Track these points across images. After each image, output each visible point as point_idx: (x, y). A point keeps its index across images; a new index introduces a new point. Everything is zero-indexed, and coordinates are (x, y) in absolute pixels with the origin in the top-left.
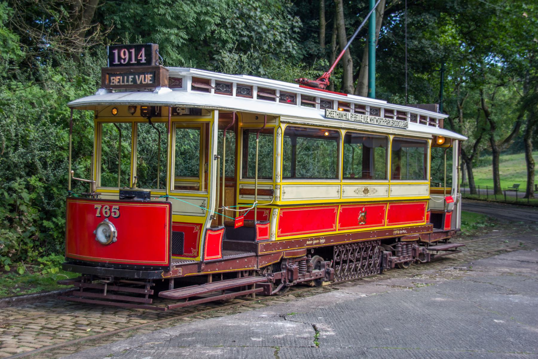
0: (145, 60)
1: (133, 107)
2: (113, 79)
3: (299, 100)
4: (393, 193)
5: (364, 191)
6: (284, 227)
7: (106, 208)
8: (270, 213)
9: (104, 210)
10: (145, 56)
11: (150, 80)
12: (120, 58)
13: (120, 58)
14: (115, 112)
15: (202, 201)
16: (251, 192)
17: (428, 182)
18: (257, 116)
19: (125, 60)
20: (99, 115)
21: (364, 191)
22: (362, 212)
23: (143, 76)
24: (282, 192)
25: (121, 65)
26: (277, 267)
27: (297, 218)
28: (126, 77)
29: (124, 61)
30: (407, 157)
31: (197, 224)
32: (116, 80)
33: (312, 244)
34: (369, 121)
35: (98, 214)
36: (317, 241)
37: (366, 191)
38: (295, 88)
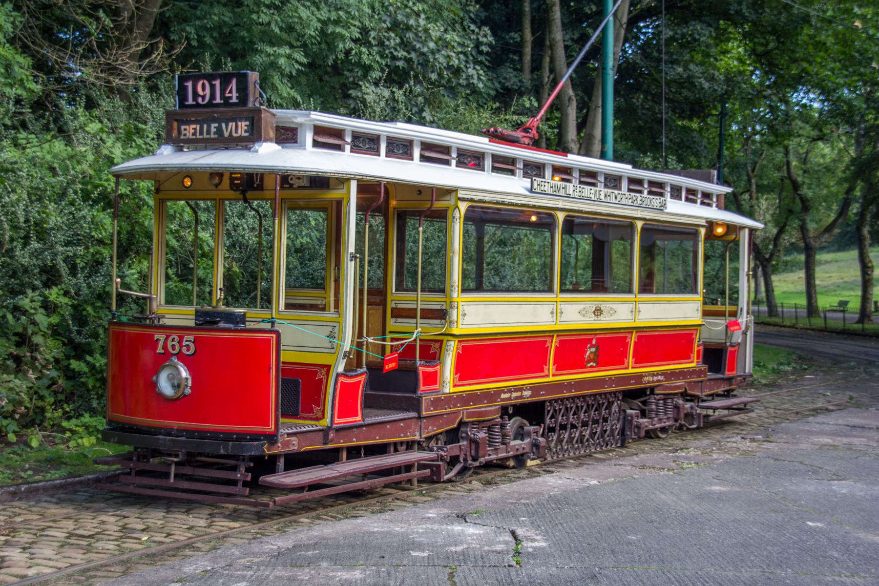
0: (237, 98)
1: (216, 174)
2: (185, 130)
3: (488, 163)
4: (642, 316)
5: (594, 312)
6: (464, 371)
7: (173, 340)
8: (441, 347)
9: (170, 343)
10: (237, 92)
11: (246, 131)
12: (196, 95)
13: (196, 95)
14: (188, 182)
15: (330, 329)
16: (410, 314)
17: (699, 297)
18: (420, 190)
19: (203, 97)
20: (162, 188)
21: (594, 312)
22: (592, 346)
23: (234, 124)
24: (460, 313)
25: (198, 105)
26: (453, 436)
27: (486, 356)
28: (205, 126)
29: (203, 100)
30: (664, 256)
31: (323, 366)
32: (189, 130)
33: (510, 399)
34: (602, 197)
35: (160, 350)
36: (519, 394)
37: (598, 312)
38: (481, 143)
